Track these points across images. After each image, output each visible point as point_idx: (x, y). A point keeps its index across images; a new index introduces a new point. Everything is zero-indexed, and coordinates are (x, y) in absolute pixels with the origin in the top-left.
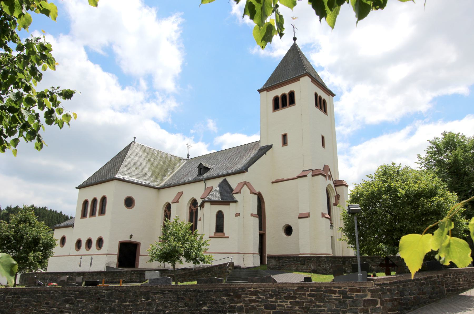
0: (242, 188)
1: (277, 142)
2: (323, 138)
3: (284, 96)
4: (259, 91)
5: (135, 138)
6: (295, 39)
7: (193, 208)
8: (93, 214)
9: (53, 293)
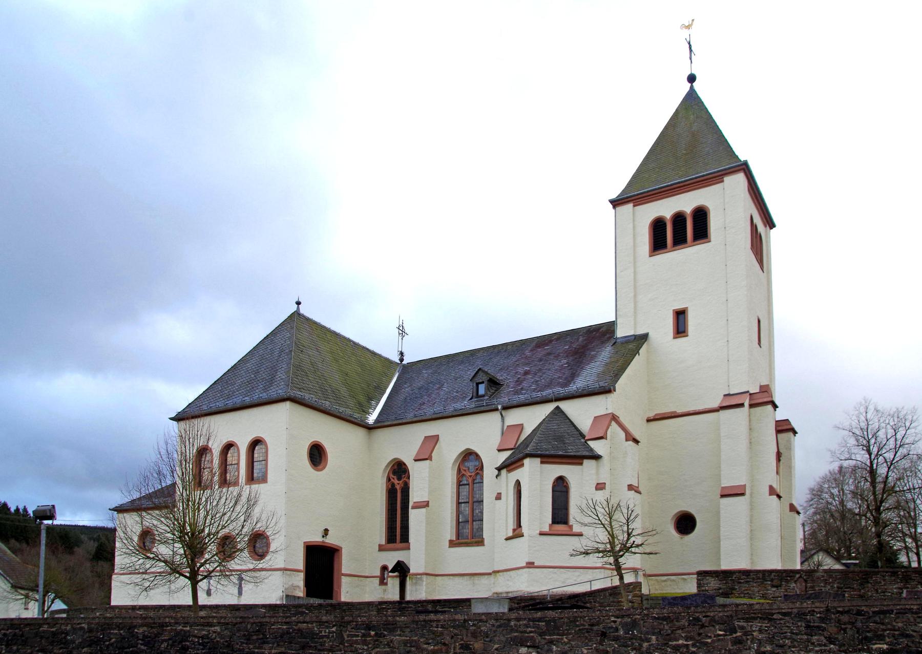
0: (608, 428)
1: (660, 329)
3: (679, 218)
5: (298, 303)
6: (692, 79)
7: (396, 482)
9: (474, 625)
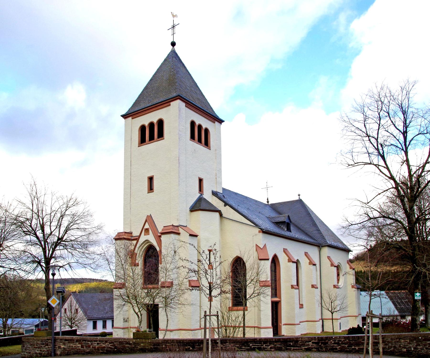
2: (201, 180)
3: (151, 125)
4: (125, 116)
6: (173, 44)
8: (152, 138)
